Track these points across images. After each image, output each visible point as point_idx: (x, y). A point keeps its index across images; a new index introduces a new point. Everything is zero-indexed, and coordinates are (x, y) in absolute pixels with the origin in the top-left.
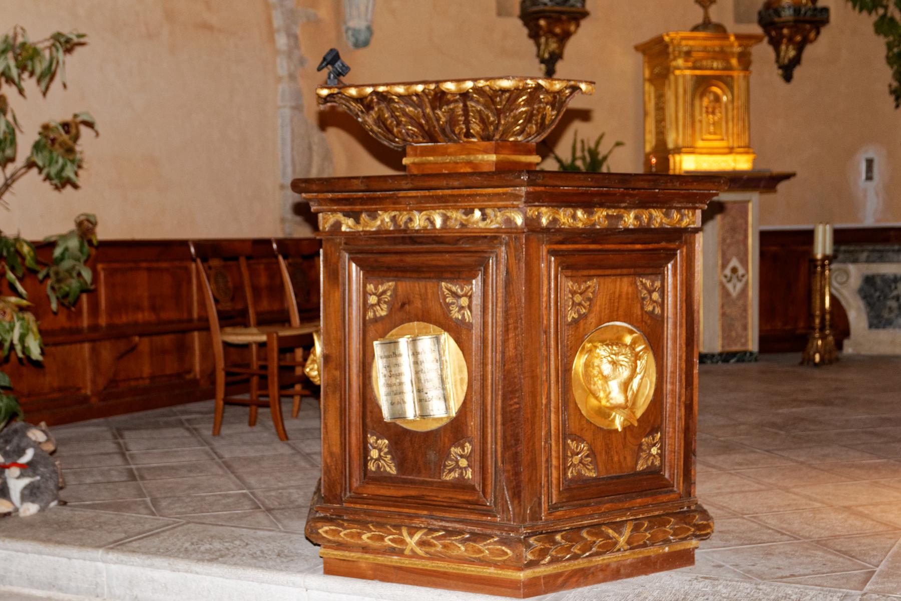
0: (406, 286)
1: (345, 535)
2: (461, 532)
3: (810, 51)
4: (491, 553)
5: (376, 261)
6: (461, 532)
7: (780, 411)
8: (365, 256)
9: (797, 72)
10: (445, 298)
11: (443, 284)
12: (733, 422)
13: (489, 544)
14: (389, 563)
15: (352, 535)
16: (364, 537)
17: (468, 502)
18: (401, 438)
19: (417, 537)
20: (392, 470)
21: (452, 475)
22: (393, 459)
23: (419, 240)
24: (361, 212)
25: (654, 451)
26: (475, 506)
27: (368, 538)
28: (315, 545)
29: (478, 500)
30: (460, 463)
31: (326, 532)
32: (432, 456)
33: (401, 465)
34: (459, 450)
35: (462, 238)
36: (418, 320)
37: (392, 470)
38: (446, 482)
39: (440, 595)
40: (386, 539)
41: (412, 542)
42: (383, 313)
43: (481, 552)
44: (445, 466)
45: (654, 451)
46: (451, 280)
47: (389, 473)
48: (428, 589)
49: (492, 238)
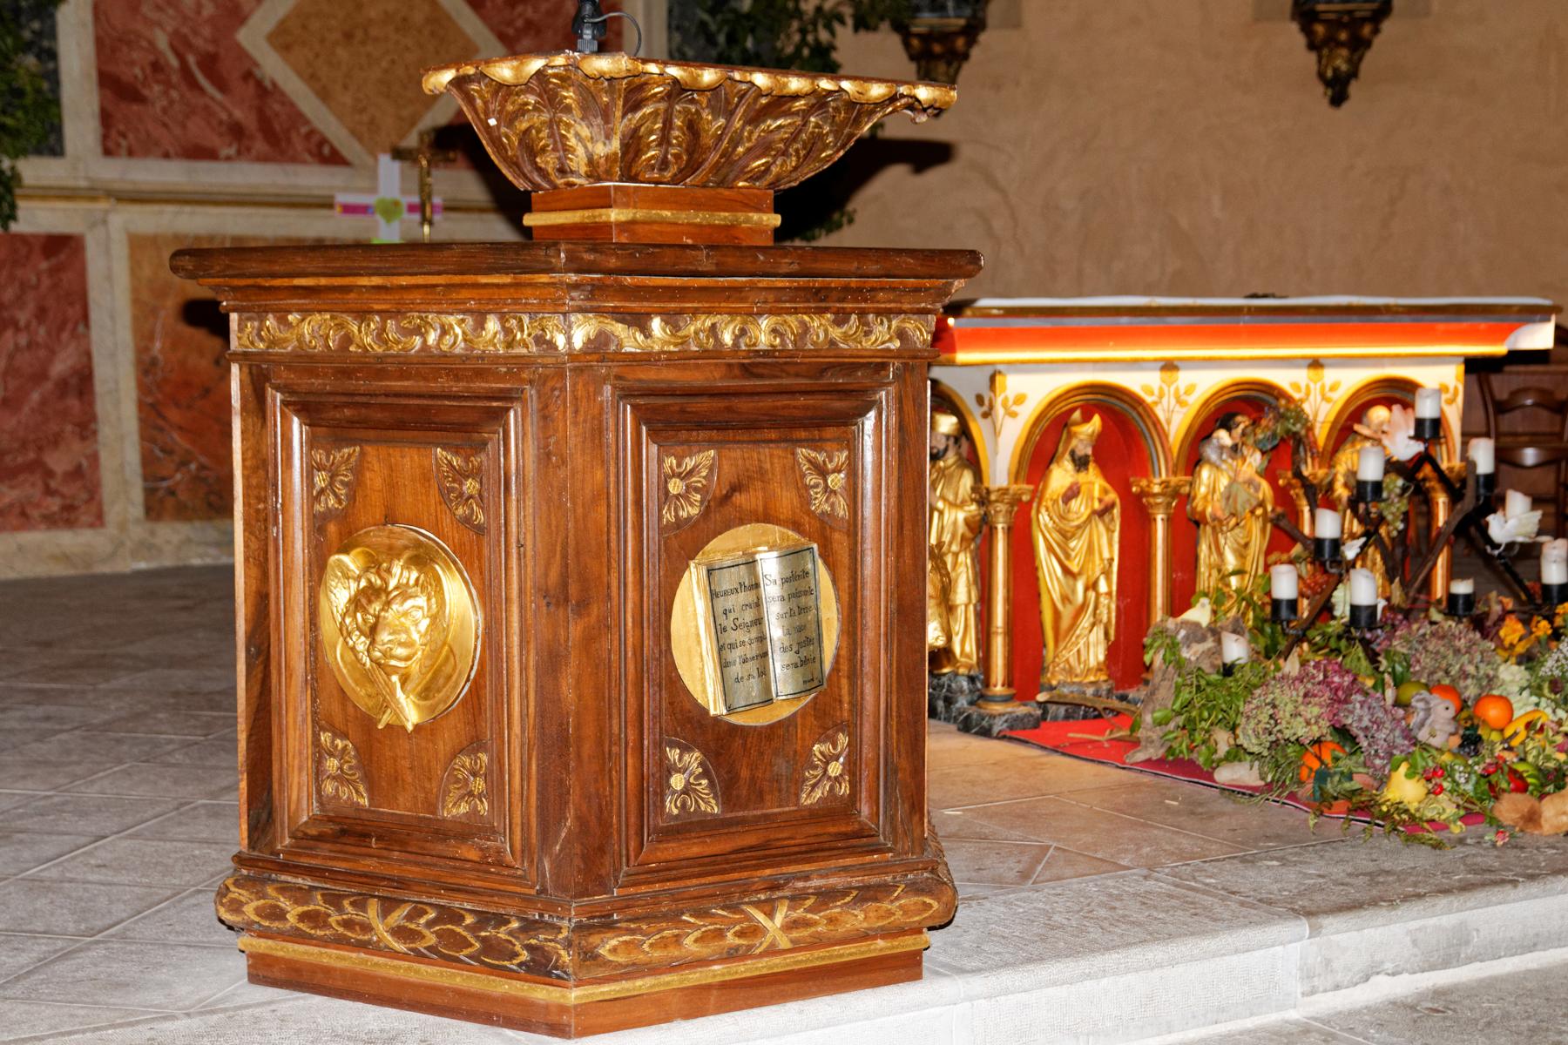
0: (740, 457)
1: (651, 945)
2: (845, 892)
3: (1370, 61)
4: (905, 913)
5: (683, 411)
6: (845, 892)
7: (283, 878)
8: (660, 401)
9: (1354, 88)
10: (803, 476)
11: (802, 452)
12: (40, 948)
13: (897, 898)
14: (709, 981)
15: (663, 944)
16: (688, 942)
17: (847, 836)
18: (720, 742)
19: (779, 918)
20: (715, 808)
21: (818, 794)
22: (712, 785)
23: (760, 370)
24: (648, 316)
25: (835, 769)
26: (858, 841)
27: (696, 941)
28: (950, 923)
29: (862, 830)
30: (827, 772)
31: (614, 950)
32: (781, 766)
33: (727, 790)
34: (826, 748)
35: (831, 366)
36: (758, 521)
37: (715, 808)
38: (810, 809)
39: (801, 1012)
40: (729, 934)
41: (774, 925)
42: (694, 511)
43: (890, 913)
44: (805, 780)
45: (835, 769)
46: (814, 444)
47: (705, 814)
48: (773, 1008)
49: (877, 366)
